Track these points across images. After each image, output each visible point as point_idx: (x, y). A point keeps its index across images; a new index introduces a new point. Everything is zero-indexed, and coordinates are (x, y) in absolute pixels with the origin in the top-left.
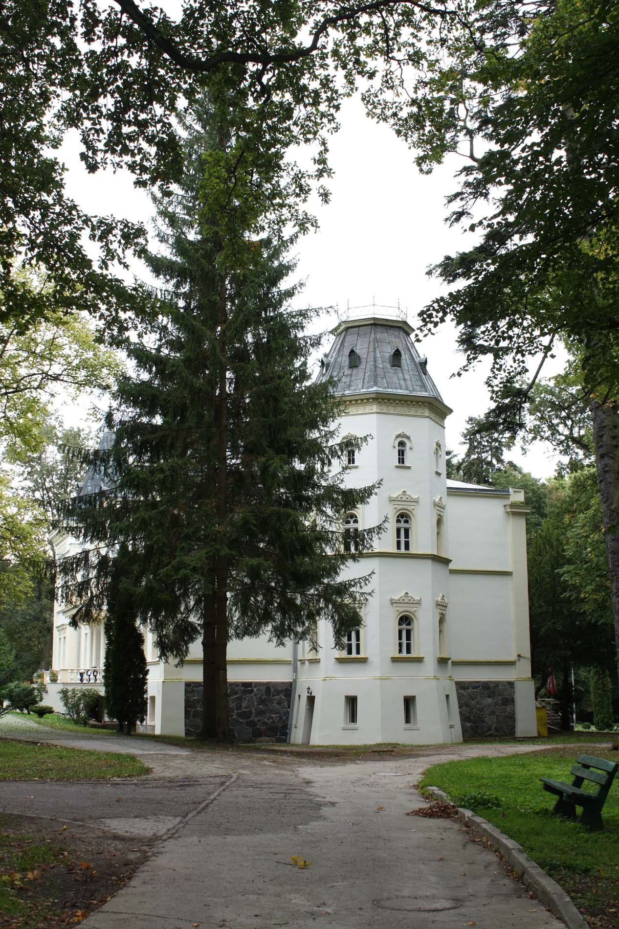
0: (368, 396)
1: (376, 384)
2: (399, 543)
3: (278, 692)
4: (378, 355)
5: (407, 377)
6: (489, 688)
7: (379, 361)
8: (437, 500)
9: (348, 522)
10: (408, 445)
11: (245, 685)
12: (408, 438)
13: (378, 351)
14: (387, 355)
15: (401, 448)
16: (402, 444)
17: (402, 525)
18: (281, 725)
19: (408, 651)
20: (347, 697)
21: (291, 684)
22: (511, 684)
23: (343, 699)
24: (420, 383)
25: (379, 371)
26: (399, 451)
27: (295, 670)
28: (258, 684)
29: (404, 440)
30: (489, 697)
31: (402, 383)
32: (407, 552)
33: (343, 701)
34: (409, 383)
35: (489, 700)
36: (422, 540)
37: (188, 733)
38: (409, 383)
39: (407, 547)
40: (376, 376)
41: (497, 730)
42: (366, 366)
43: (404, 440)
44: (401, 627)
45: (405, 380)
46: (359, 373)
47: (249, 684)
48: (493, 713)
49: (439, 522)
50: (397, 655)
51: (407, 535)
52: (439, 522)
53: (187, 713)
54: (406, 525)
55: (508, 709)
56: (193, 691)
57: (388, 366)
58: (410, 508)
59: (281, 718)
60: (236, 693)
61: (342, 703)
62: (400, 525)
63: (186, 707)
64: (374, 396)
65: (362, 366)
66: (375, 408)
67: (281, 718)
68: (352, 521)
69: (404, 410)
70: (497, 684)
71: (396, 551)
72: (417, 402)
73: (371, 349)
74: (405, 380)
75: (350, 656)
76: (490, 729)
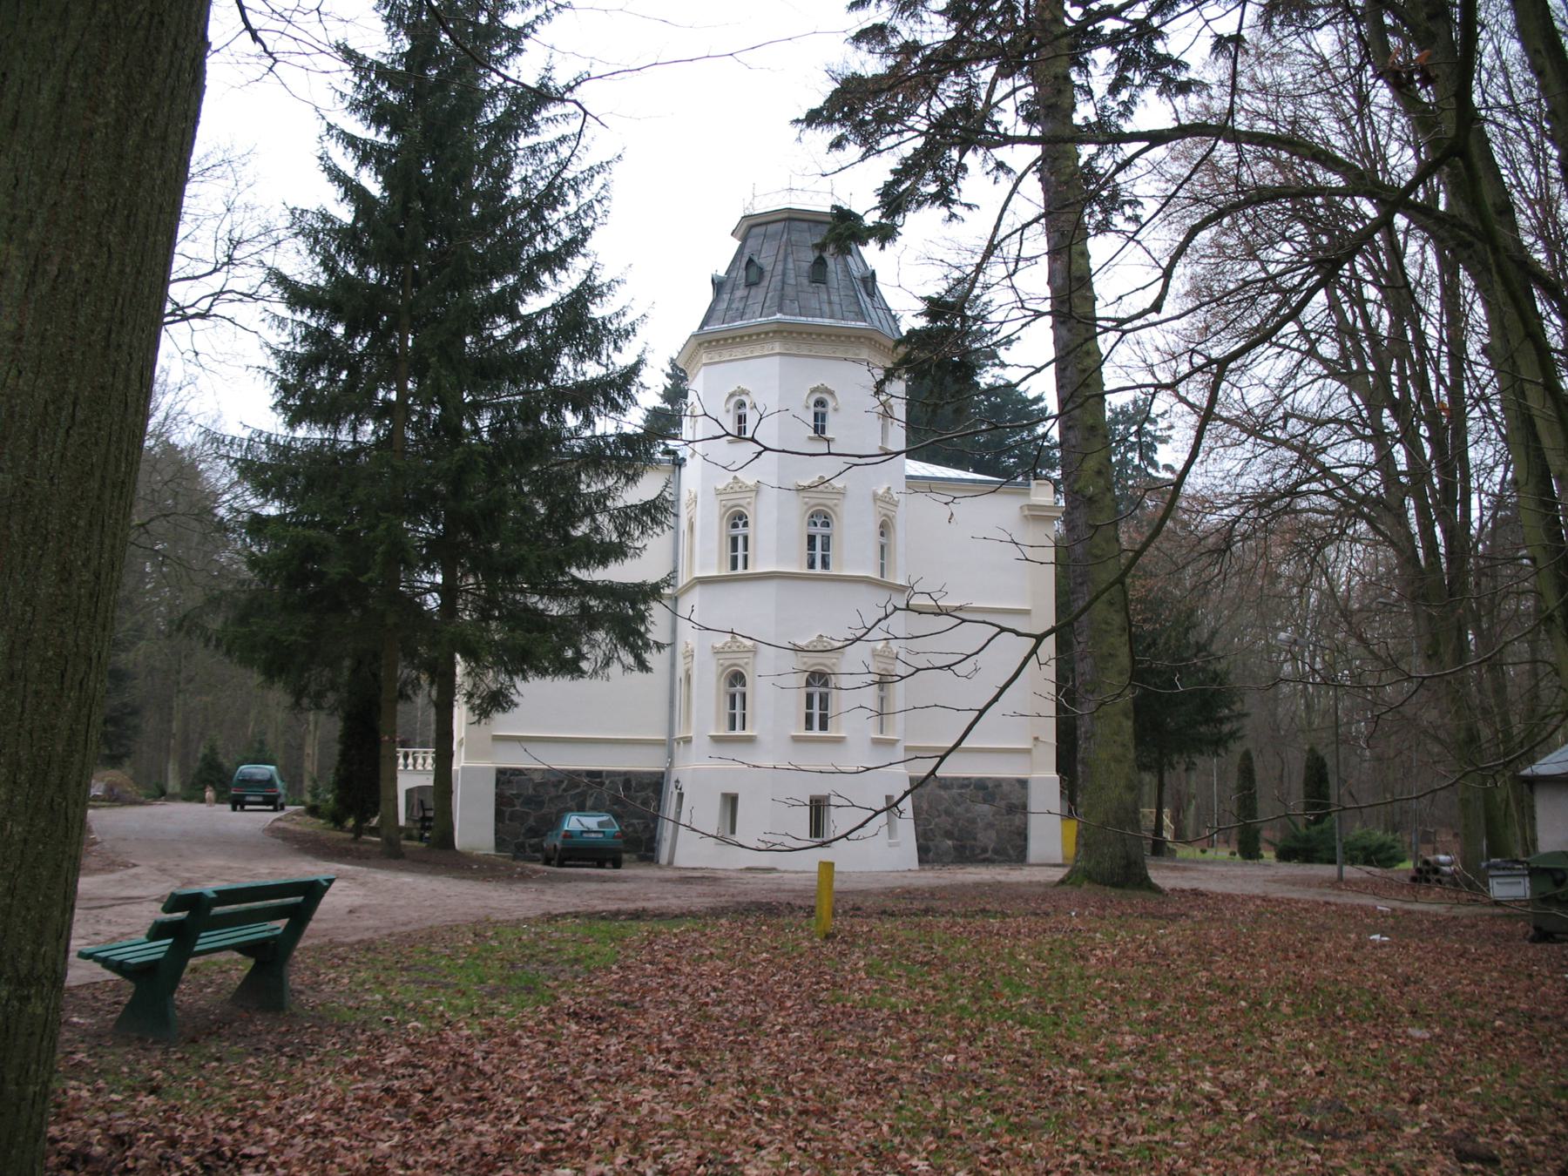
0: (767, 328)
1: (780, 310)
2: (734, 559)
3: (642, 787)
4: (790, 266)
5: (835, 298)
6: (985, 788)
7: (791, 274)
8: (881, 492)
9: (735, 526)
10: (831, 404)
11: (592, 774)
12: (831, 393)
13: (790, 260)
14: (806, 266)
15: (819, 409)
16: (820, 403)
17: (819, 531)
18: (645, 837)
19: (823, 727)
20: (725, 796)
21: (662, 774)
22: (1023, 783)
23: (718, 799)
24: (854, 308)
25: (789, 291)
26: (816, 414)
27: (671, 755)
28: (610, 774)
29: (744, 398)
30: (985, 801)
31: (826, 307)
32: (825, 572)
33: (718, 800)
34: (836, 307)
35: (986, 807)
36: (854, 552)
37: (500, 843)
38: (836, 307)
39: (825, 565)
40: (782, 298)
41: (995, 851)
42: (771, 283)
43: (744, 398)
44: (733, 690)
45: (830, 303)
46: (758, 293)
47: (598, 774)
48: (991, 825)
49: (885, 529)
50: (724, 732)
51: (826, 546)
52: (885, 529)
53: (499, 815)
54: (825, 531)
55: (1017, 820)
56: (510, 782)
57: (805, 282)
58: (829, 503)
59: (647, 826)
60: (578, 786)
61: (717, 802)
62: (735, 532)
63: (497, 805)
64: (774, 327)
65: (765, 283)
66: (777, 347)
67: (647, 826)
68: (740, 523)
69: (738, 352)
70: (998, 783)
71: (806, 570)
72: (829, 336)
73: (781, 257)
74: (830, 303)
75: (810, 733)
76: (985, 850)
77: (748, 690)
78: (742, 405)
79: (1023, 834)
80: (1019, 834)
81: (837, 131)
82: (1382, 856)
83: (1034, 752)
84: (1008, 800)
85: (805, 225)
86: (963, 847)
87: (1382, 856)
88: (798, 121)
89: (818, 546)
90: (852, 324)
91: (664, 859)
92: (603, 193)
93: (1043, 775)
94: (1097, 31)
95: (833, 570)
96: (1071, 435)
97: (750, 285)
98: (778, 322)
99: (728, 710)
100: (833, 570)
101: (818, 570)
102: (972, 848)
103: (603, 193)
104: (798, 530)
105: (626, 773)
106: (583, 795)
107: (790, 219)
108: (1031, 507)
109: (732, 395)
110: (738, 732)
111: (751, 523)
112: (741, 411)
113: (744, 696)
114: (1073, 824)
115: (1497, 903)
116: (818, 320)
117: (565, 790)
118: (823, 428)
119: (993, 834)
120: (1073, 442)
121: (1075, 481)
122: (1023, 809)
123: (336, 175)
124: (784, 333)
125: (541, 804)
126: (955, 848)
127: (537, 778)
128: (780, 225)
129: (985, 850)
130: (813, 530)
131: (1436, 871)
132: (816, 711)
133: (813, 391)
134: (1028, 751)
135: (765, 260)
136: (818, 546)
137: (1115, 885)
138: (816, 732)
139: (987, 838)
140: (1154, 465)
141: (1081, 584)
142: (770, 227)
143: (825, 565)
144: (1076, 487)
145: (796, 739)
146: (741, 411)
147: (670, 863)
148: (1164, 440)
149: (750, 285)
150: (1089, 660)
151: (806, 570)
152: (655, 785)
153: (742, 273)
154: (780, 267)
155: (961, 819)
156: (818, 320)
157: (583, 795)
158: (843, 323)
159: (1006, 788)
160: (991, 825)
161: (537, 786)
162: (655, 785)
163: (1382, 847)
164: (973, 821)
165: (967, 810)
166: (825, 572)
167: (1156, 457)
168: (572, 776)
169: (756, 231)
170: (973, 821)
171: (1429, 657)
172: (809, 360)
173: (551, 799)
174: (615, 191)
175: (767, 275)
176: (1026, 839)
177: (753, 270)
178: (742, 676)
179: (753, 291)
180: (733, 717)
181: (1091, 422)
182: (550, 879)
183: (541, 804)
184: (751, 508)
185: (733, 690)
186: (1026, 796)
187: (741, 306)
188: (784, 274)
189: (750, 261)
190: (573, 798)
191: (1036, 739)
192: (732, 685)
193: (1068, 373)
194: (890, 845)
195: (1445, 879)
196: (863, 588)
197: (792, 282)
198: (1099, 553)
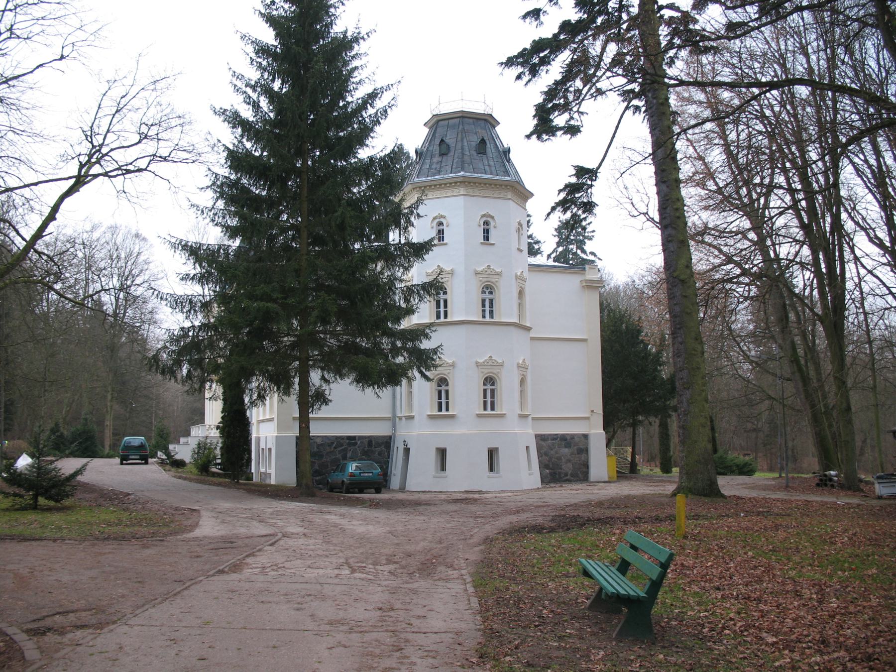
1: (463, 169)
3: (379, 445)
4: (466, 144)
5: (492, 163)
6: (566, 440)
7: (466, 149)
8: (519, 274)
10: (492, 224)
11: (350, 438)
12: (492, 218)
13: (465, 140)
14: (474, 144)
15: (486, 227)
16: (486, 223)
17: (487, 296)
19: (493, 409)
21: (390, 437)
22: (586, 436)
23: (435, 450)
24: (503, 169)
25: (466, 158)
27: (394, 426)
28: (361, 438)
30: (566, 447)
31: (487, 168)
32: (491, 320)
34: (493, 168)
35: (566, 450)
38: (493, 168)
40: (463, 162)
41: (572, 475)
43: (442, 220)
44: (485, 387)
45: (489, 166)
46: (448, 160)
47: (354, 438)
48: (569, 461)
49: (521, 293)
50: (435, 412)
51: (491, 305)
52: (521, 293)
54: (491, 296)
55: (583, 456)
58: (494, 280)
60: (342, 445)
61: (433, 453)
64: (461, 179)
65: (452, 154)
66: (462, 191)
69: (443, 193)
70: (573, 436)
71: (481, 319)
73: (459, 139)
74: (489, 166)
76: (566, 475)
77: (450, 388)
78: (441, 224)
79: (586, 466)
80: (584, 465)
81: (520, 69)
82: (745, 470)
83: (592, 419)
84: (577, 446)
85: (471, 121)
86: (555, 473)
87: (745, 470)
88: (502, 64)
89: (488, 305)
90: (502, 178)
91: (395, 482)
92: (393, 102)
93: (596, 431)
94: (662, 16)
95: (496, 319)
96: (670, 245)
97: (442, 155)
98: (463, 177)
99: (437, 400)
100: (496, 319)
101: (488, 319)
102: (560, 474)
103: (393, 102)
104: (476, 297)
105: (369, 437)
106: (345, 450)
107: (463, 117)
108: (587, 281)
109: (435, 218)
110: (444, 412)
111: (448, 291)
112: (441, 228)
113: (447, 392)
114: (614, 459)
115: (880, 498)
116: (484, 176)
117: (335, 448)
118: (488, 237)
119: (570, 465)
120: (672, 249)
121: (674, 271)
122: (586, 451)
123: (237, 90)
124: (466, 182)
125: (322, 456)
126: (550, 474)
127: (319, 441)
128: (457, 120)
129: (566, 475)
130: (484, 296)
131: (831, 480)
132: (489, 399)
133: (483, 216)
134: (588, 418)
135: (450, 140)
136: (488, 305)
137: (705, 495)
138: (489, 412)
139: (567, 468)
140: (584, 251)
141: (679, 329)
142: (451, 121)
143: (492, 316)
144: (675, 275)
145: (479, 416)
146: (441, 228)
147: (402, 489)
148: (590, 239)
149: (442, 155)
150: (686, 371)
151: (481, 319)
152: (386, 443)
153: (437, 148)
154: (459, 145)
155: (561, 459)
156: (484, 176)
157: (345, 450)
158: (497, 178)
159: (576, 439)
160: (569, 461)
161: (319, 446)
162: (386, 443)
163: (746, 464)
164: (559, 459)
165: (556, 453)
166: (491, 320)
167: (585, 248)
168: (352, 440)
169: (441, 123)
170: (559, 459)
171: (792, 362)
172: (492, 200)
173: (327, 453)
174: (400, 101)
175: (452, 150)
176: (588, 468)
177: (444, 146)
178: (446, 380)
179: (445, 158)
180: (440, 404)
181: (681, 238)
182: (575, 506)
183: (322, 456)
184: (449, 283)
185: (440, 388)
186: (587, 444)
187: (438, 166)
188: (462, 149)
189: (442, 141)
190: (340, 452)
191: (592, 411)
192: (439, 385)
193: (668, 211)
194: (530, 474)
195: (836, 484)
196: (512, 328)
197: (468, 153)
198: (689, 311)
